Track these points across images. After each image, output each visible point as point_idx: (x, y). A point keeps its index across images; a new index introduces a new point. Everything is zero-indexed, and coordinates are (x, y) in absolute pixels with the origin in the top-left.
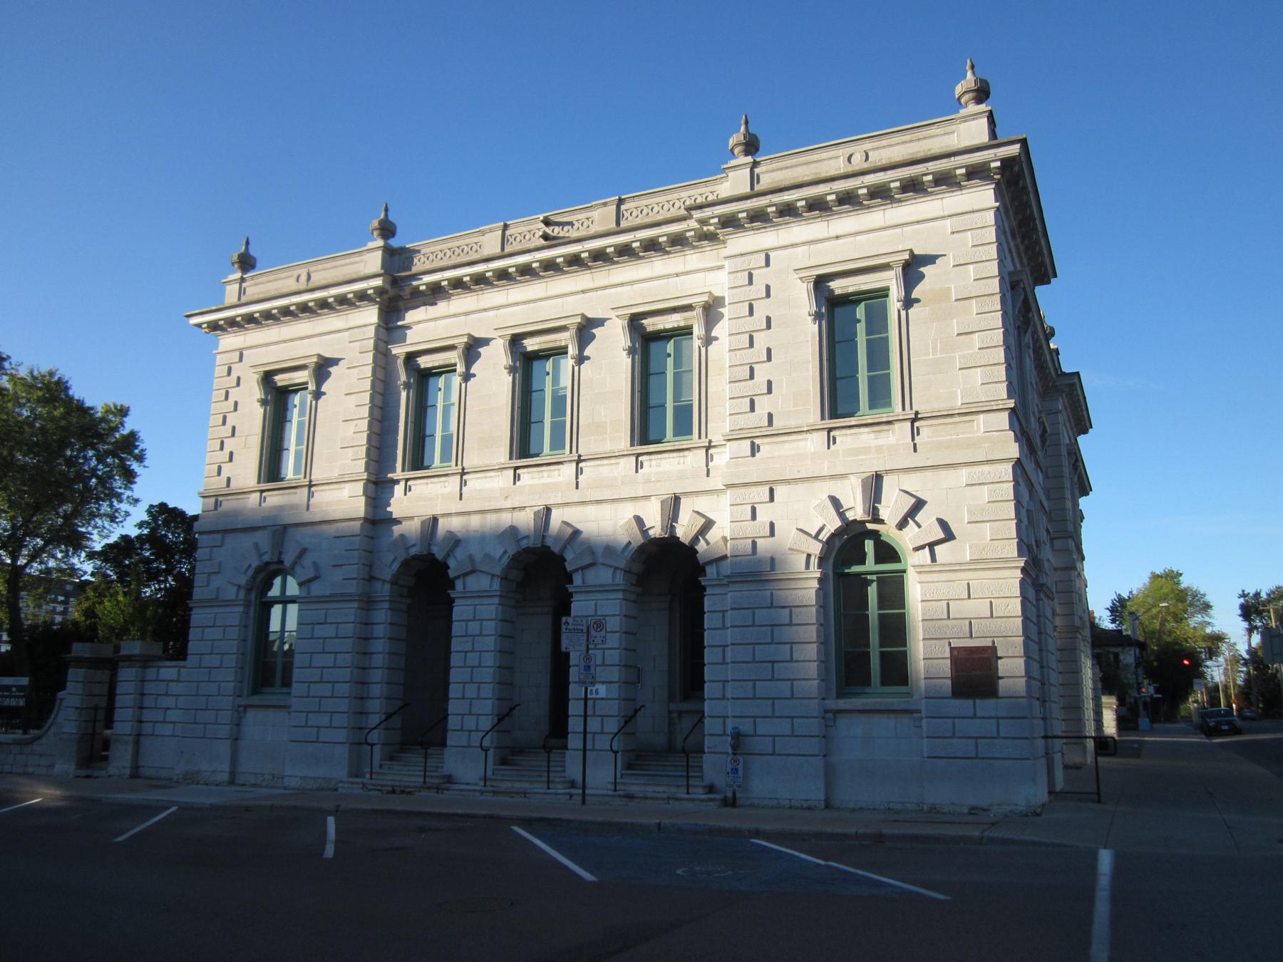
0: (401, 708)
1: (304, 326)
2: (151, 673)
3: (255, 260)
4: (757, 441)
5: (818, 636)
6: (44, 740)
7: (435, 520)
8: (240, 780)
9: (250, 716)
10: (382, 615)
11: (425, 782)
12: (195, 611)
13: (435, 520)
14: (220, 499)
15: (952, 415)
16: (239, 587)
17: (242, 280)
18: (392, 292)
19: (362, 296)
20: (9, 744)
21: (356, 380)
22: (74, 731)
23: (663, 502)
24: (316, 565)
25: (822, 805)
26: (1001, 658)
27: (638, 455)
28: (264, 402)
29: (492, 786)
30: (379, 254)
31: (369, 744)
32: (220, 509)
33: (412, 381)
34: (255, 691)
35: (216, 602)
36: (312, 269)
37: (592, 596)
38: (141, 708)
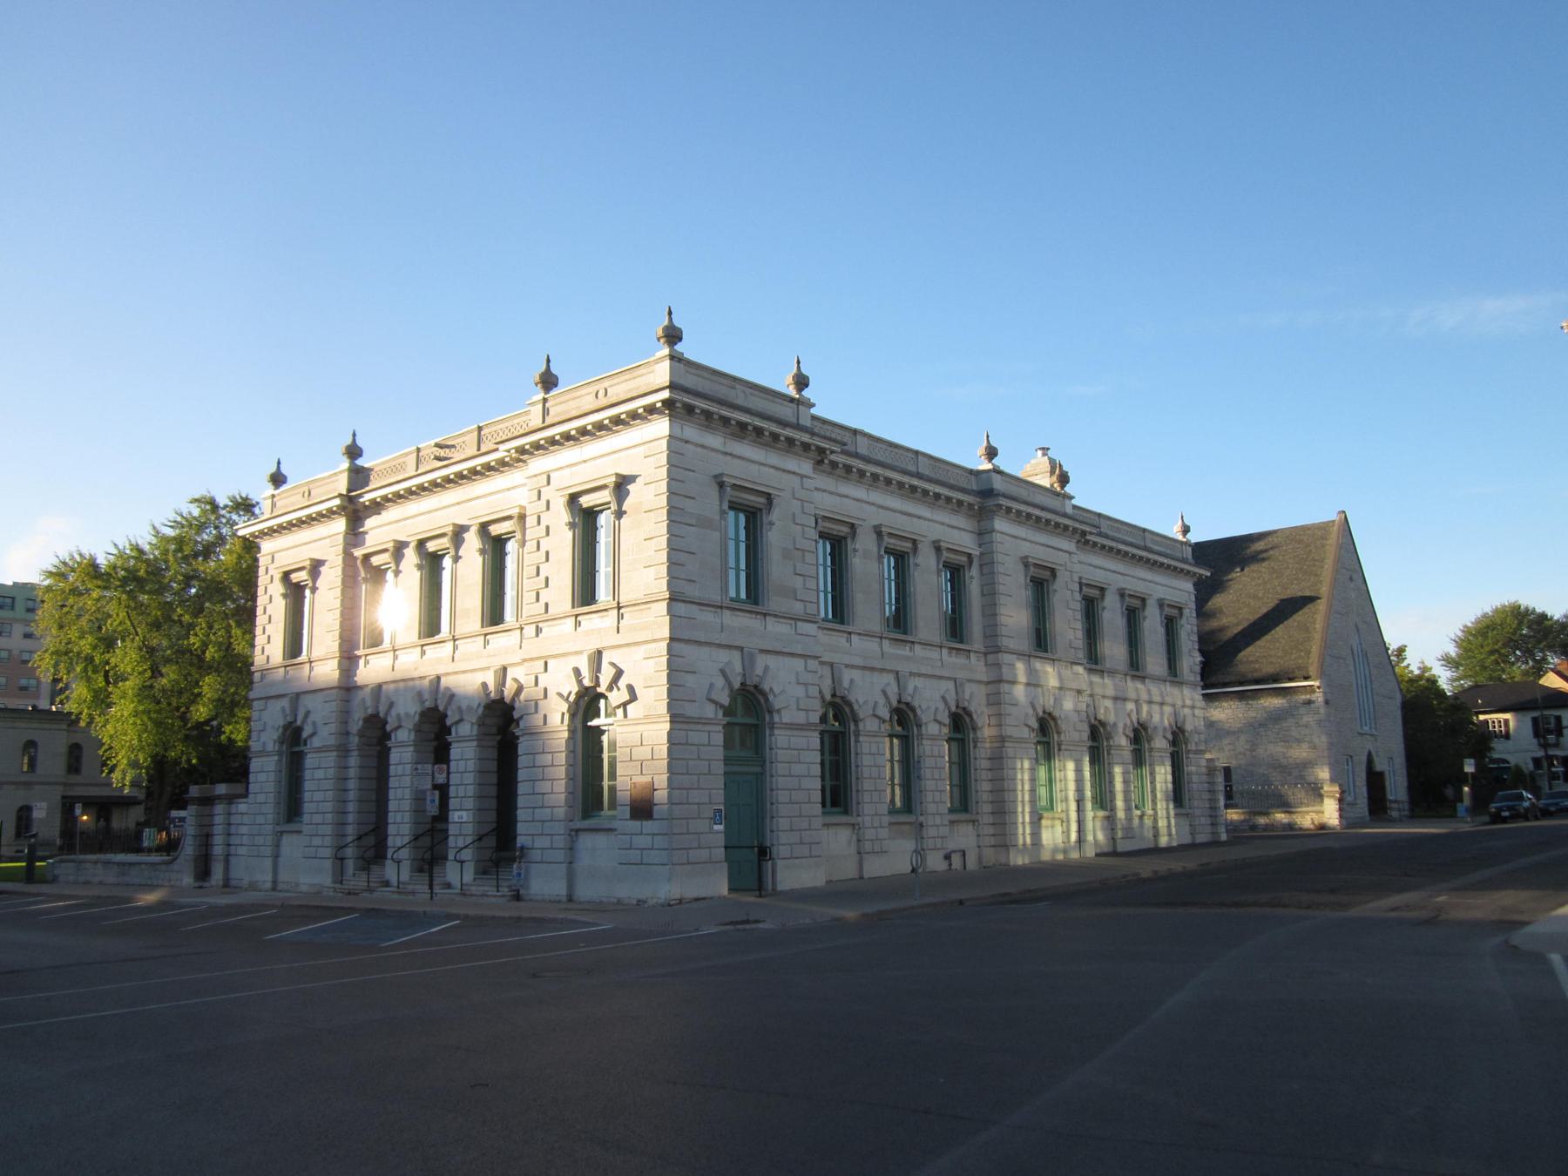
0: (373, 830)
1: (591, 448)
2: (233, 808)
3: (680, 331)
4: (540, 625)
5: (566, 775)
6: (178, 861)
7: (438, 678)
8: (280, 887)
9: (286, 839)
10: (353, 761)
11: (368, 886)
12: (253, 760)
13: (438, 678)
14: (265, 672)
15: (638, 604)
16: (472, 724)
17: (545, 400)
18: (351, 507)
19: (651, 410)
20: (159, 864)
21: (653, 496)
22: (192, 853)
23: (495, 672)
24: (631, 689)
25: (564, 899)
26: (656, 790)
27: (486, 635)
28: (572, 525)
29: (404, 888)
30: (667, 363)
31: (458, 861)
32: (265, 681)
33: (577, 520)
34: (586, 815)
35: (263, 753)
36: (311, 486)
37: (707, 728)
38: (229, 835)
